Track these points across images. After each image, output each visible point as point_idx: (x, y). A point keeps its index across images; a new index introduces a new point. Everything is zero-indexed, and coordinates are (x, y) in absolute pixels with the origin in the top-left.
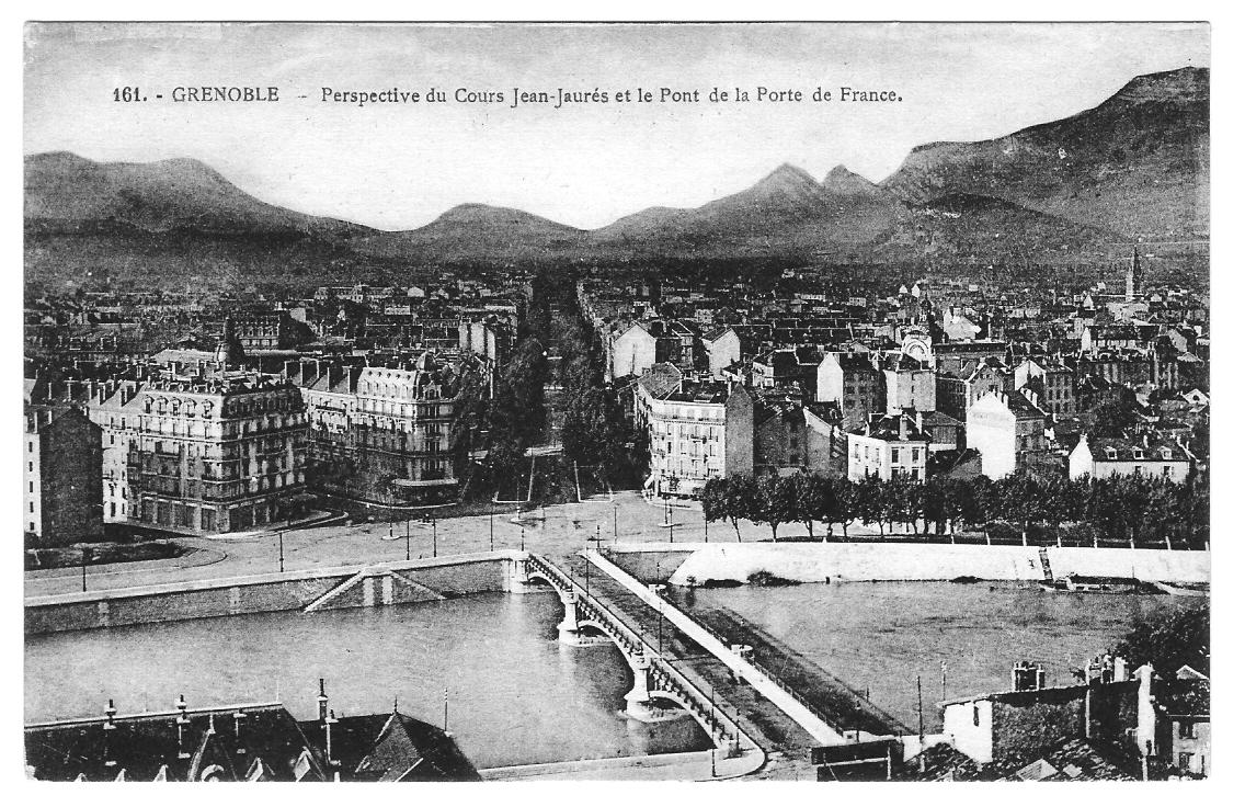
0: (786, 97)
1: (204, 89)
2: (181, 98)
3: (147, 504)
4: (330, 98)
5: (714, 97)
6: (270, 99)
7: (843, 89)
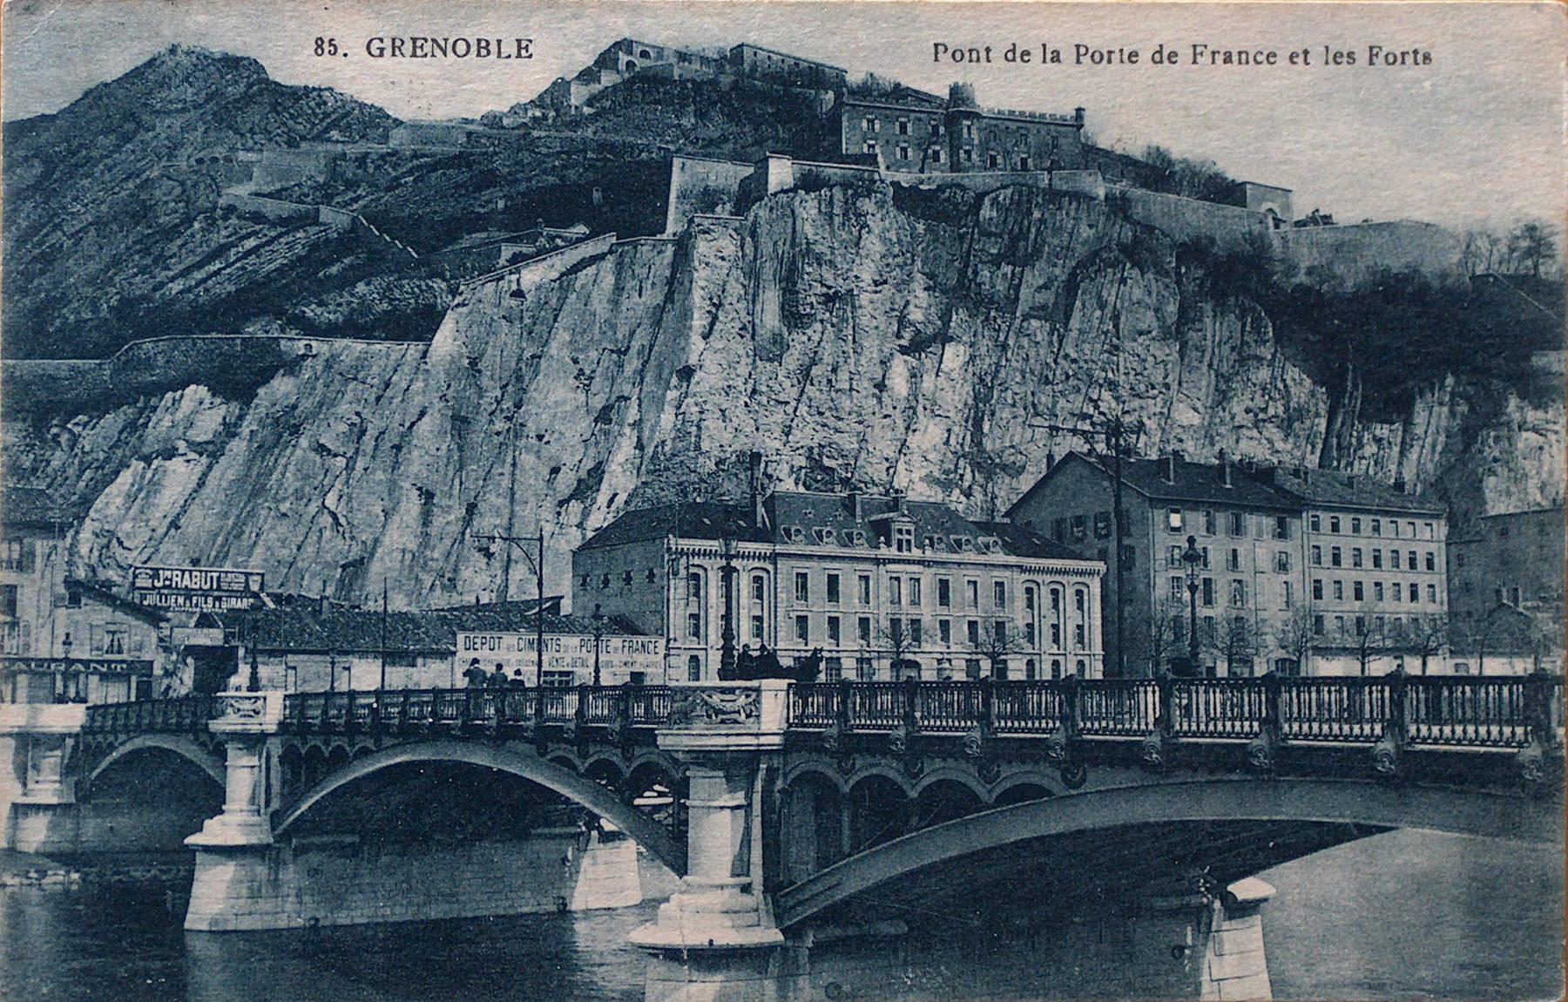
0: (1410, 59)
1: (414, 40)
2: (378, 52)
3: (47, 680)
4: (1086, 60)
5: (1010, 55)
6: (519, 56)
7: (1195, 47)
